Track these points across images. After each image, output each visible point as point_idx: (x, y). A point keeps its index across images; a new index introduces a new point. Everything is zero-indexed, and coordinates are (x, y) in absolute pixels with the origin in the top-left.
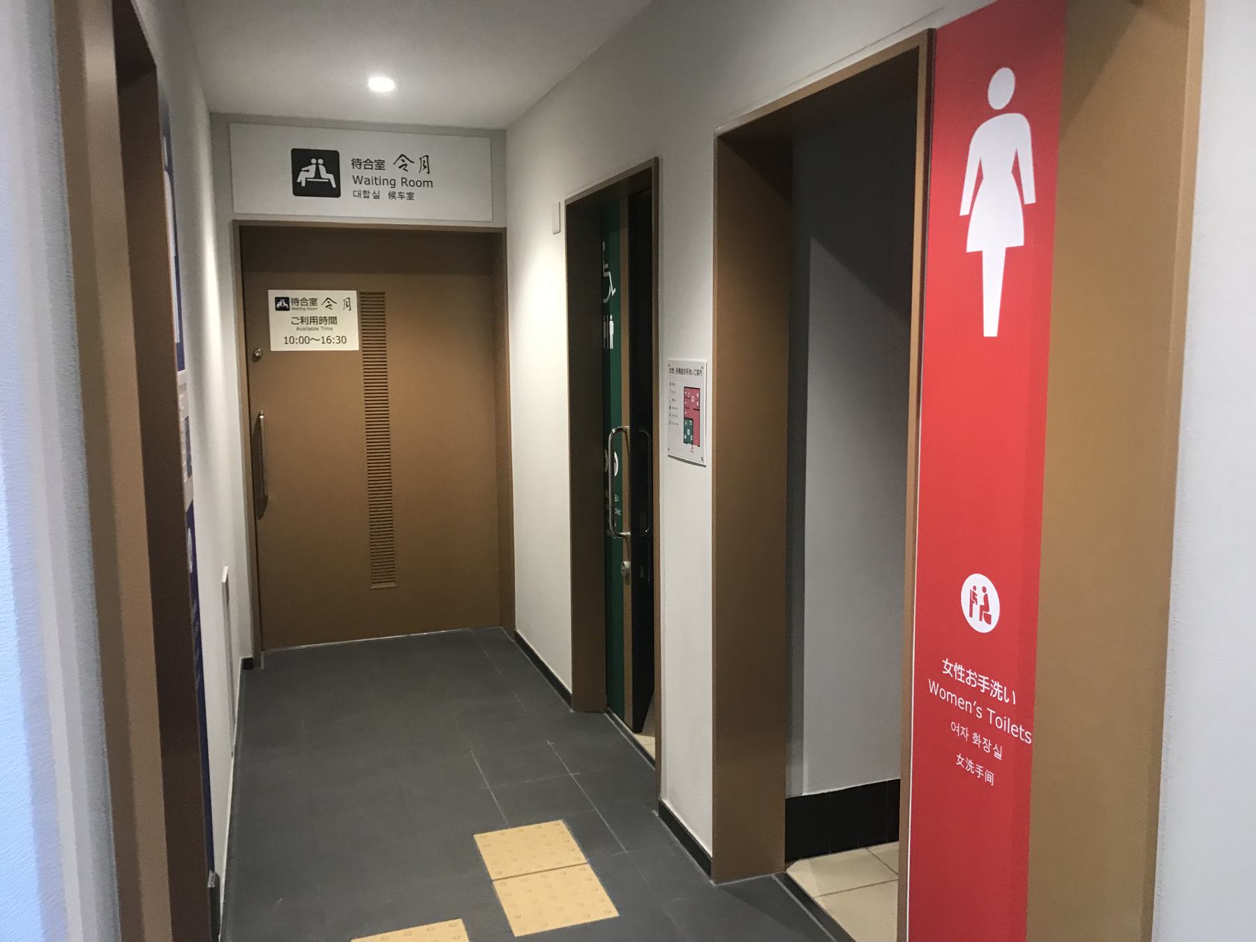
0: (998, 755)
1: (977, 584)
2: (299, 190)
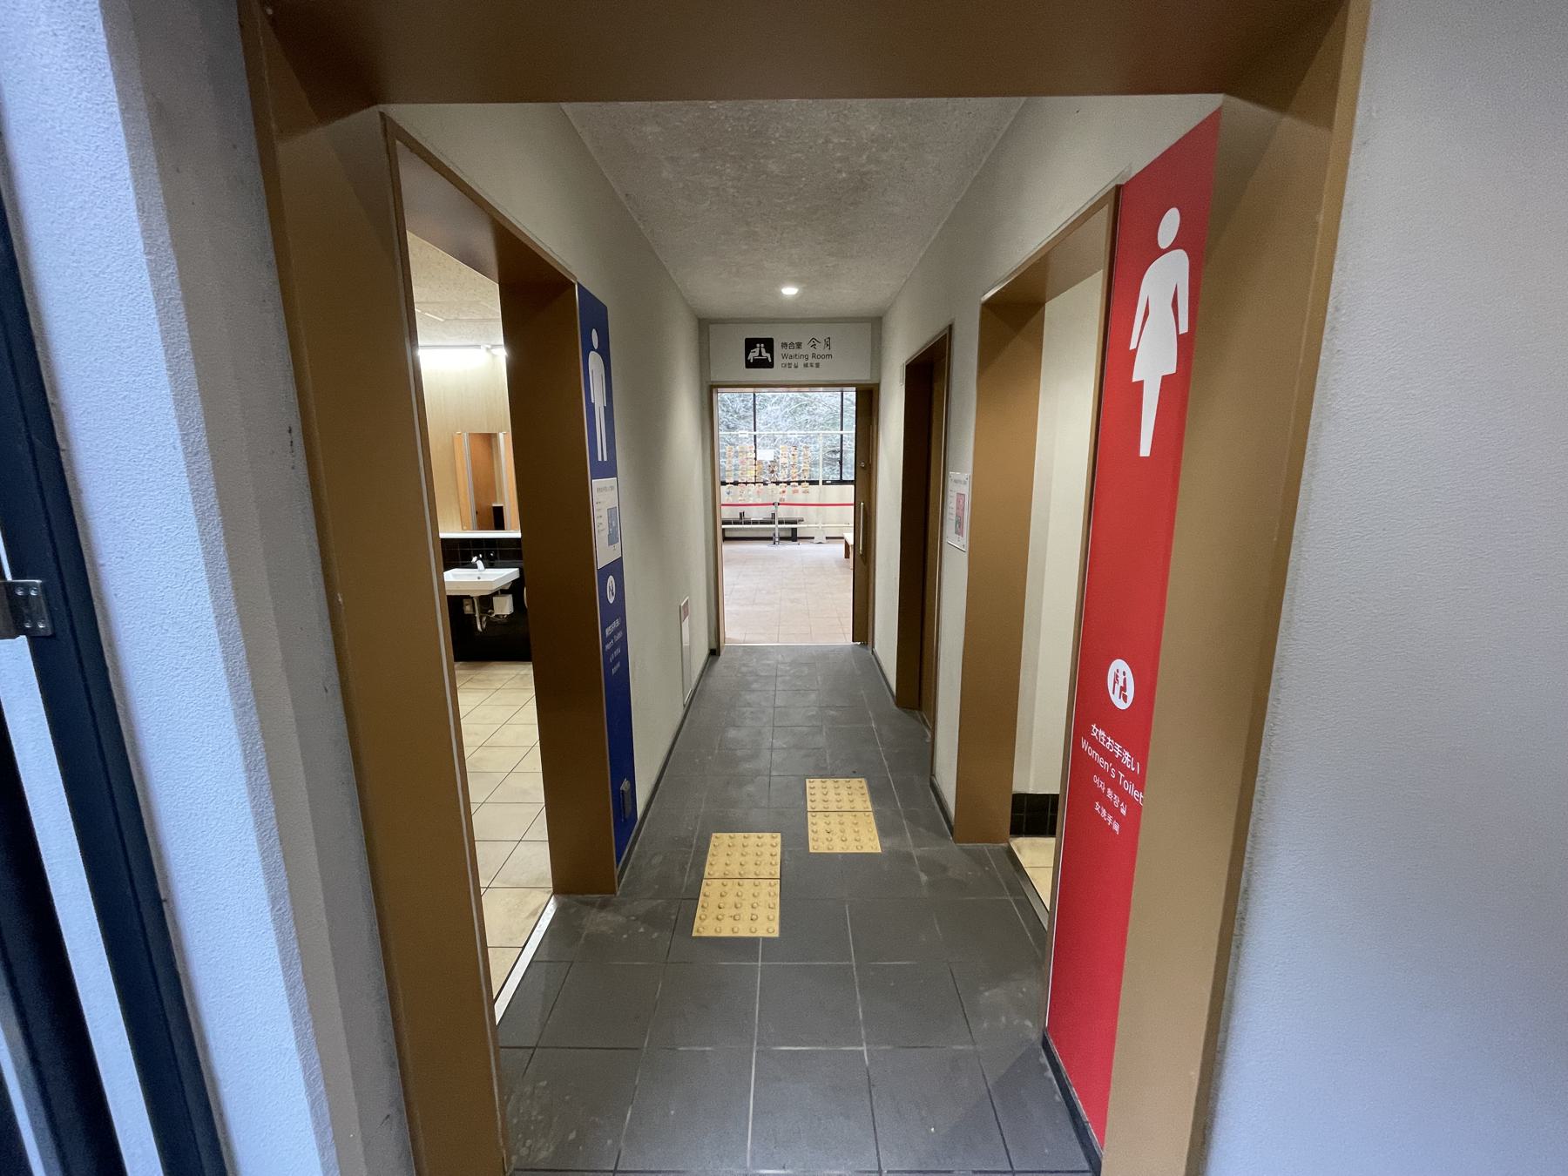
0: (1123, 811)
1: (1119, 667)
2: (749, 365)
